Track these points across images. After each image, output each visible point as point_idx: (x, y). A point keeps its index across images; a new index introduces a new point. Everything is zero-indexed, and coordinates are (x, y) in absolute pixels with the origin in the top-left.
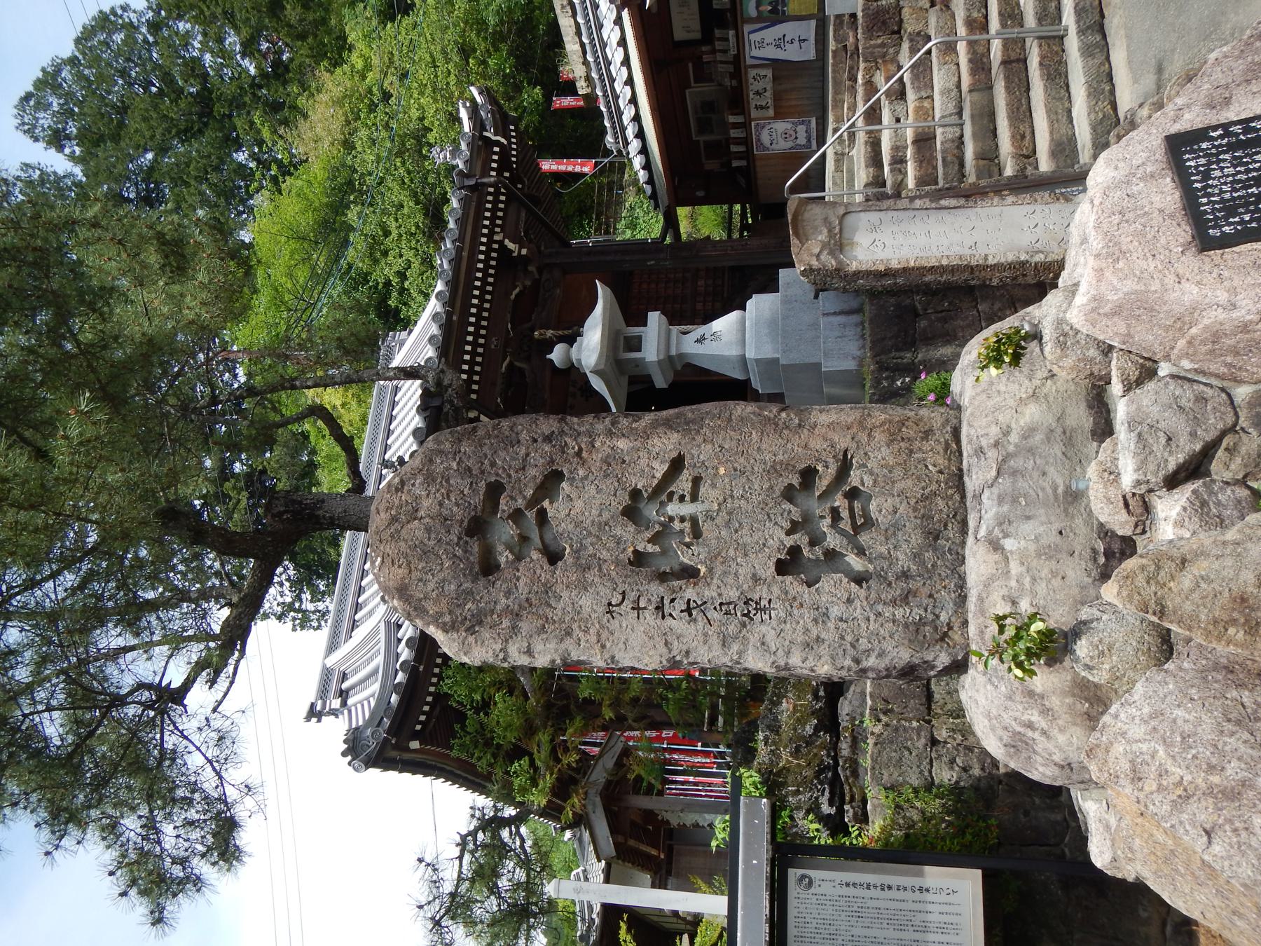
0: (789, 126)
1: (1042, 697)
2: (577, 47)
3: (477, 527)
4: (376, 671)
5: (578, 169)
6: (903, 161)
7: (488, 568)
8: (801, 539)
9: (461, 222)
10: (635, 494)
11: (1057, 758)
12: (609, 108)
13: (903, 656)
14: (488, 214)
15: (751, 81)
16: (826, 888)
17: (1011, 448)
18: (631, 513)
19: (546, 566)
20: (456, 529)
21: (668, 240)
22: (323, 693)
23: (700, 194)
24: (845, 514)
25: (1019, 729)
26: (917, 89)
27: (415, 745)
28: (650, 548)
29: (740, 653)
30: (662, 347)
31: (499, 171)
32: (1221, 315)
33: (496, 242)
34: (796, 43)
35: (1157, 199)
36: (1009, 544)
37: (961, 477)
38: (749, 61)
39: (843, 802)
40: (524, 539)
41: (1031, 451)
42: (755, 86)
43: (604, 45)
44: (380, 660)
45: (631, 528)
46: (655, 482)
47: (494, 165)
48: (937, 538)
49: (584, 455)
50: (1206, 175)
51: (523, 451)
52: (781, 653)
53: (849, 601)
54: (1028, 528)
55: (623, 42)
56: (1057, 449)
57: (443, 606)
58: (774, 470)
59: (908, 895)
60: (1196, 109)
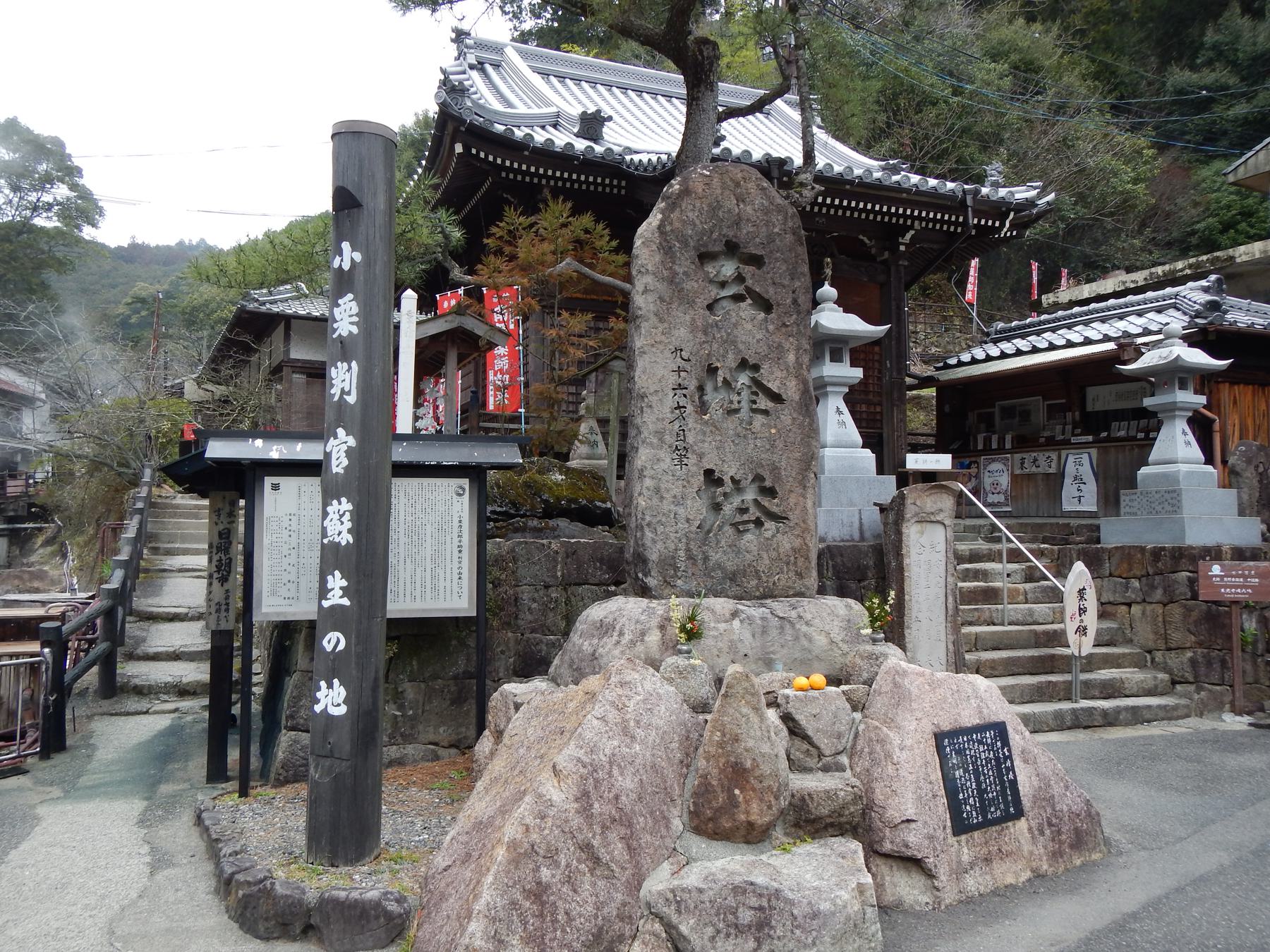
0: (1004, 487)
1: (642, 640)
2: (1086, 295)
3: (732, 249)
4: (510, 105)
5: (970, 287)
6: (976, 578)
7: (704, 257)
8: (728, 486)
9: (934, 193)
10: (756, 368)
11: (601, 650)
12: (1029, 326)
13: (653, 556)
14: (939, 216)
15: (1047, 454)
16: (457, 506)
17: (798, 626)
18: (743, 364)
19: (706, 303)
20: (731, 234)
21: (908, 380)
22: (481, 45)
23: (947, 409)
24: (745, 517)
25: (617, 628)
26: (1034, 590)
27: (459, 148)
28: (720, 379)
29: (651, 444)
30: (834, 380)
31: (977, 226)
32: (897, 742)
33: (913, 223)
34: (1077, 494)
35: (966, 713)
36: (736, 623)
37: (771, 597)
38: (1064, 453)
39: (495, 521)
40: (723, 285)
41: (797, 638)
42: (1042, 457)
43: (1086, 324)
44: (521, 109)
45: (734, 365)
46: (765, 383)
47: (983, 222)
48: (731, 580)
49: (784, 330)
50: (980, 742)
51: (786, 282)
52: (652, 472)
53: (688, 520)
54: (747, 635)
55: (1088, 342)
56: (797, 655)
57: (677, 224)
58: (775, 469)
59: (456, 565)
60: (1022, 742)
